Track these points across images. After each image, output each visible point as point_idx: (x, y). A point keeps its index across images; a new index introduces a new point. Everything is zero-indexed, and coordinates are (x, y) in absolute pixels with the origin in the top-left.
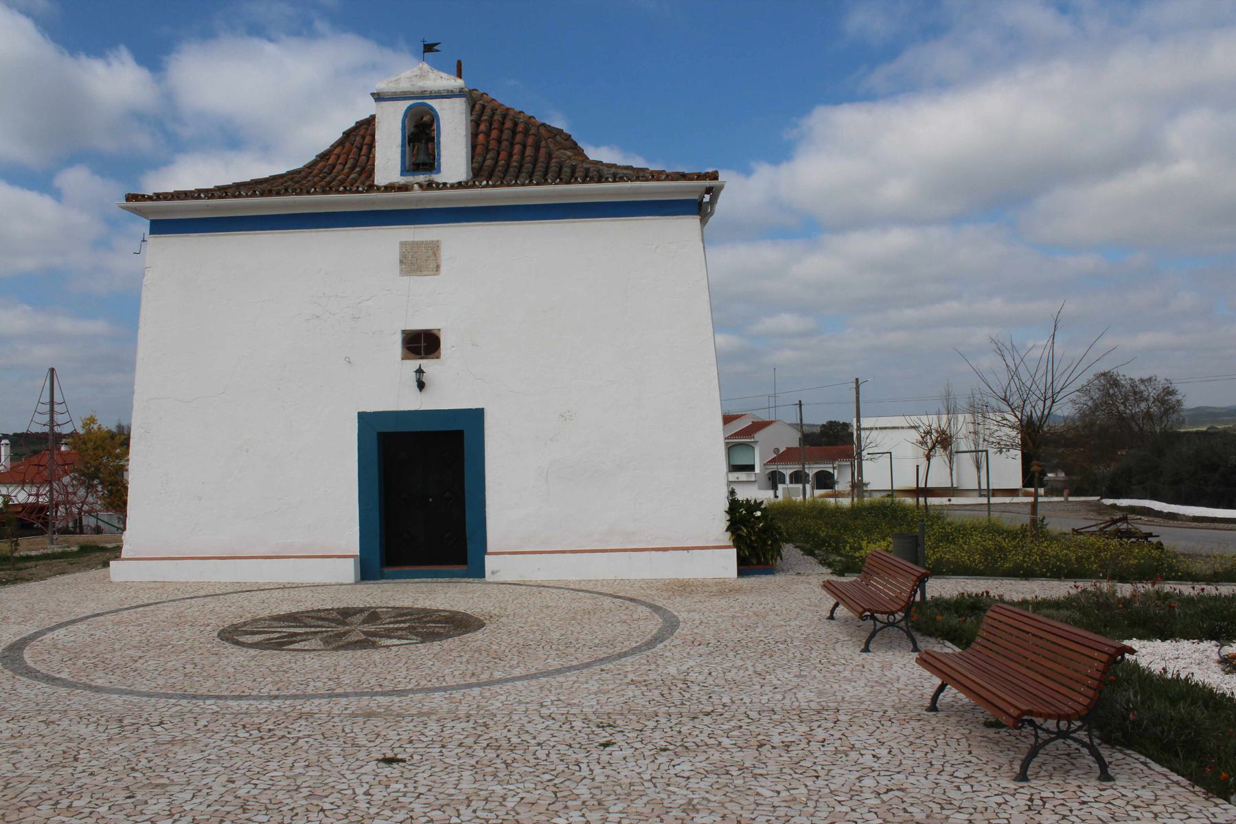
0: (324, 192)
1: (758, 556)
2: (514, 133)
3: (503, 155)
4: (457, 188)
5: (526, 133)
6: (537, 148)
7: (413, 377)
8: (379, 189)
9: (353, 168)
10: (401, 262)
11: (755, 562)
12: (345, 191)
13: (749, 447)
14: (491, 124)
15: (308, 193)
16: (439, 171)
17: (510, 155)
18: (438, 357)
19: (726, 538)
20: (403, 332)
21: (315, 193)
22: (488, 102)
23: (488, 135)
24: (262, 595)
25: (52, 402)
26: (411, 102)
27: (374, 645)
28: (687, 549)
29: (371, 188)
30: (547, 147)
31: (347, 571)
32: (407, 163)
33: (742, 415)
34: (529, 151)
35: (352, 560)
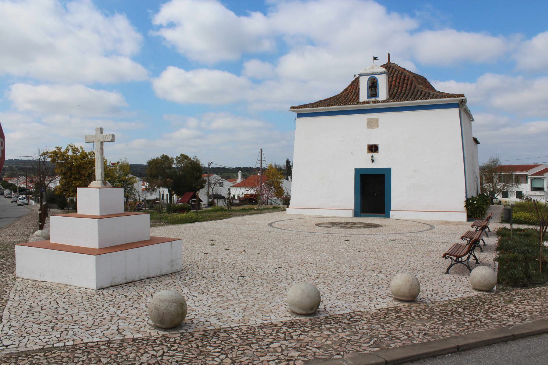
0: (345, 105)
1: (474, 216)
2: (404, 79)
3: (400, 88)
4: (383, 103)
5: (408, 79)
6: (411, 84)
7: (370, 158)
8: (360, 103)
9: (354, 94)
10: (367, 124)
11: (473, 217)
12: (351, 104)
13: (542, 179)
14: (397, 77)
15: (340, 105)
16: (378, 97)
17: (402, 88)
18: (378, 153)
19: (464, 209)
20: (368, 145)
21: (342, 105)
22: (398, 68)
23: (396, 81)
24: (327, 218)
25: (261, 160)
26: (370, 76)
27: (352, 228)
28: (451, 212)
29: (358, 103)
30: (415, 84)
31: (351, 214)
32: (369, 95)
33: (540, 165)
34: (408, 86)
35: (352, 211)
